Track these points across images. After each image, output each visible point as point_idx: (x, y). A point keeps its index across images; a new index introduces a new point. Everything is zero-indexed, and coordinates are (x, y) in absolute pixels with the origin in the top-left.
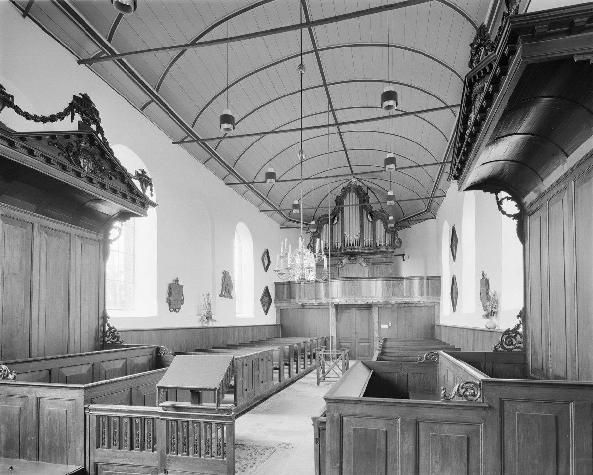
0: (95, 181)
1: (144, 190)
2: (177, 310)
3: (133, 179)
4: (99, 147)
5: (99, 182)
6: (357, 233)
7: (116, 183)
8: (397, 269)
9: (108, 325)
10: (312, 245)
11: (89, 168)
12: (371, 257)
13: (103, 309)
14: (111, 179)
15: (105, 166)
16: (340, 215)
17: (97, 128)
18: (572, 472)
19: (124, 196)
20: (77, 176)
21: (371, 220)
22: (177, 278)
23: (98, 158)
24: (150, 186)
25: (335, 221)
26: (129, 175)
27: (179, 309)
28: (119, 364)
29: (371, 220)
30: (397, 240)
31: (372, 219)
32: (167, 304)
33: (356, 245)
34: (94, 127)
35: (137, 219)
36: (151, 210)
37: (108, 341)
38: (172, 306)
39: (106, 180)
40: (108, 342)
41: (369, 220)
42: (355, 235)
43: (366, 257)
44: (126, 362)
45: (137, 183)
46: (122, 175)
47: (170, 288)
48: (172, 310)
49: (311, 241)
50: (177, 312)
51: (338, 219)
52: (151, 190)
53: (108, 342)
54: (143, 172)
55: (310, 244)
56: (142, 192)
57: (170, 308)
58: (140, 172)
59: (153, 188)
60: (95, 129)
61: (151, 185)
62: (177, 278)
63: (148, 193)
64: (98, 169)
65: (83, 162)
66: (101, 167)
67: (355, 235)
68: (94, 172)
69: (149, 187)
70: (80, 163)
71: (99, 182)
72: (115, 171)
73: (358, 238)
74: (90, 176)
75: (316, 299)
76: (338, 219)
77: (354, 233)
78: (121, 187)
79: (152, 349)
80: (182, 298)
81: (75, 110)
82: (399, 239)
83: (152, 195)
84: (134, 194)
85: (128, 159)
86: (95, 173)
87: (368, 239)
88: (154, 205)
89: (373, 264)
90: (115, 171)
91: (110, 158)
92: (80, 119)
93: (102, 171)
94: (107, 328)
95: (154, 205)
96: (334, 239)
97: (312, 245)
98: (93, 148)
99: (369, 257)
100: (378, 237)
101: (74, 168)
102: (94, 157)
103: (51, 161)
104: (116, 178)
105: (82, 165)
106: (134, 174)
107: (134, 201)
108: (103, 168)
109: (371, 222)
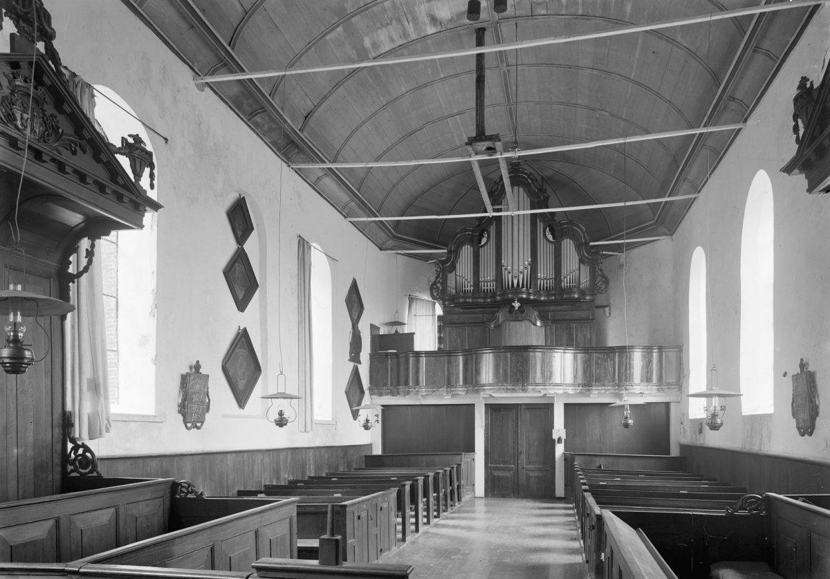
0: (45, 158)
1: (138, 175)
2: (199, 425)
3: (118, 156)
4: (53, 90)
5: (53, 160)
6: (526, 263)
7: (83, 161)
8: (600, 334)
9: (73, 441)
10: (439, 285)
11: (32, 130)
12: (552, 308)
13: (60, 410)
14: (74, 153)
15: (65, 126)
16: (493, 229)
17: (46, 48)
18: (417, 372)
19: (102, 188)
20: (36, 159)
21: (551, 239)
22: (198, 362)
23: (50, 109)
24: (149, 168)
25: (484, 241)
26: (109, 146)
27: (202, 423)
28: (105, 516)
29: (551, 239)
30: (599, 278)
31: (554, 238)
32: (180, 415)
33: (523, 287)
34: (41, 46)
35: (122, 233)
36: (149, 217)
37: (72, 471)
38: (188, 419)
39: (66, 156)
40: (73, 475)
41: (547, 240)
42: (521, 267)
43: (542, 308)
44: (117, 512)
45: (124, 162)
46: (97, 146)
47: (184, 379)
48: (189, 425)
49: (437, 278)
50: (198, 428)
51: (489, 238)
52: (152, 176)
53: (73, 475)
54: (137, 138)
55: (435, 283)
56: (133, 180)
57: (185, 422)
58: (131, 140)
59: (155, 171)
60: (43, 50)
61: (152, 166)
62: (198, 362)
63: (144, 182)
64: (51, 130)
65: (22, 118)
66: (56, 129)
67: (521, 267)
68: (43, 138)
69: (147, 171)
70: (16, 120)
71: (53, 160)
72: (82, 137)
73: (527, 272)
74: (38, 147)
75: (448, 387)
76: (489, 238)
77: (521, 263)
78: (100, 173)
79: (162, 487)
80: (207, 401)
81: (4, 11)
82: (603, 276)
83: (152, 187)
84: (117, 183)
85: (113, 118)
86: (44, 141)
87: (545, 273)
88: (156, 206)
89: (554, 321)
90: (82, 137)
91: (73, 112)
92: (15, 30)
93: (59, 137)
94: (70, 446)
95: (156, 206)
96: (481, 274)
97: (439, 285)
98: (41, 90)
99: (547, 308)
100: (564, 271)
101: (116, 189)
102: (42, 109)
103: (42, 156)
104: (84, 152)
105: (19, 123)
106: (118, 144)
107: (120, 198)
108: (60, 131)
109: (551, 242)
